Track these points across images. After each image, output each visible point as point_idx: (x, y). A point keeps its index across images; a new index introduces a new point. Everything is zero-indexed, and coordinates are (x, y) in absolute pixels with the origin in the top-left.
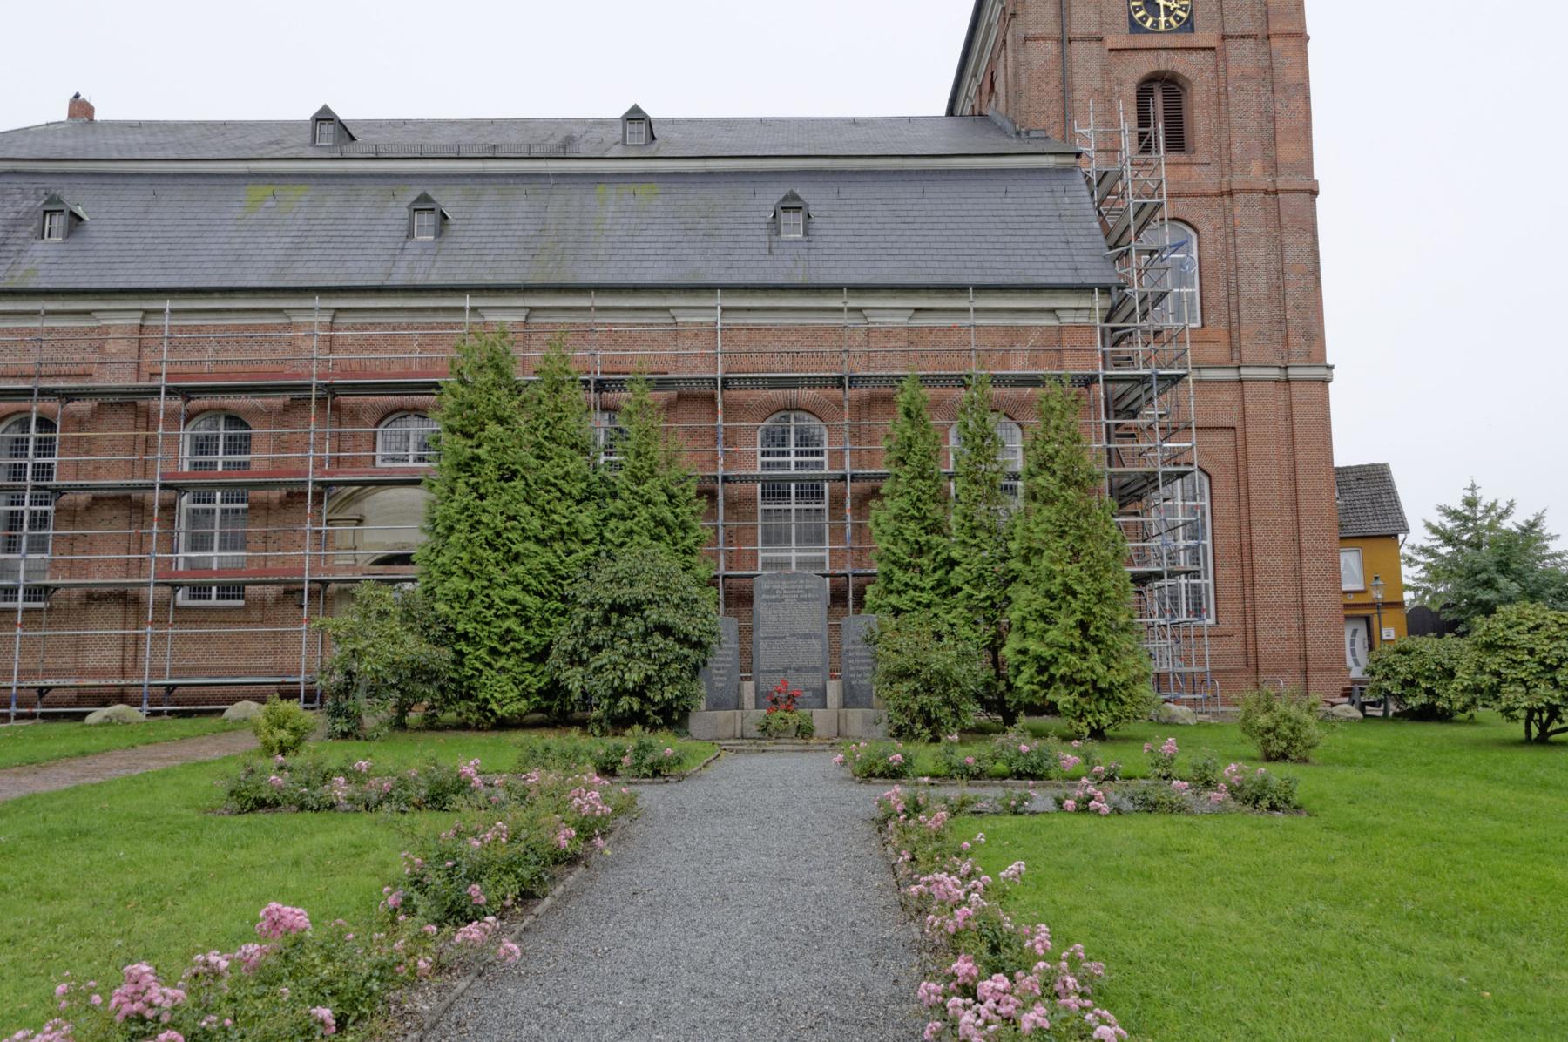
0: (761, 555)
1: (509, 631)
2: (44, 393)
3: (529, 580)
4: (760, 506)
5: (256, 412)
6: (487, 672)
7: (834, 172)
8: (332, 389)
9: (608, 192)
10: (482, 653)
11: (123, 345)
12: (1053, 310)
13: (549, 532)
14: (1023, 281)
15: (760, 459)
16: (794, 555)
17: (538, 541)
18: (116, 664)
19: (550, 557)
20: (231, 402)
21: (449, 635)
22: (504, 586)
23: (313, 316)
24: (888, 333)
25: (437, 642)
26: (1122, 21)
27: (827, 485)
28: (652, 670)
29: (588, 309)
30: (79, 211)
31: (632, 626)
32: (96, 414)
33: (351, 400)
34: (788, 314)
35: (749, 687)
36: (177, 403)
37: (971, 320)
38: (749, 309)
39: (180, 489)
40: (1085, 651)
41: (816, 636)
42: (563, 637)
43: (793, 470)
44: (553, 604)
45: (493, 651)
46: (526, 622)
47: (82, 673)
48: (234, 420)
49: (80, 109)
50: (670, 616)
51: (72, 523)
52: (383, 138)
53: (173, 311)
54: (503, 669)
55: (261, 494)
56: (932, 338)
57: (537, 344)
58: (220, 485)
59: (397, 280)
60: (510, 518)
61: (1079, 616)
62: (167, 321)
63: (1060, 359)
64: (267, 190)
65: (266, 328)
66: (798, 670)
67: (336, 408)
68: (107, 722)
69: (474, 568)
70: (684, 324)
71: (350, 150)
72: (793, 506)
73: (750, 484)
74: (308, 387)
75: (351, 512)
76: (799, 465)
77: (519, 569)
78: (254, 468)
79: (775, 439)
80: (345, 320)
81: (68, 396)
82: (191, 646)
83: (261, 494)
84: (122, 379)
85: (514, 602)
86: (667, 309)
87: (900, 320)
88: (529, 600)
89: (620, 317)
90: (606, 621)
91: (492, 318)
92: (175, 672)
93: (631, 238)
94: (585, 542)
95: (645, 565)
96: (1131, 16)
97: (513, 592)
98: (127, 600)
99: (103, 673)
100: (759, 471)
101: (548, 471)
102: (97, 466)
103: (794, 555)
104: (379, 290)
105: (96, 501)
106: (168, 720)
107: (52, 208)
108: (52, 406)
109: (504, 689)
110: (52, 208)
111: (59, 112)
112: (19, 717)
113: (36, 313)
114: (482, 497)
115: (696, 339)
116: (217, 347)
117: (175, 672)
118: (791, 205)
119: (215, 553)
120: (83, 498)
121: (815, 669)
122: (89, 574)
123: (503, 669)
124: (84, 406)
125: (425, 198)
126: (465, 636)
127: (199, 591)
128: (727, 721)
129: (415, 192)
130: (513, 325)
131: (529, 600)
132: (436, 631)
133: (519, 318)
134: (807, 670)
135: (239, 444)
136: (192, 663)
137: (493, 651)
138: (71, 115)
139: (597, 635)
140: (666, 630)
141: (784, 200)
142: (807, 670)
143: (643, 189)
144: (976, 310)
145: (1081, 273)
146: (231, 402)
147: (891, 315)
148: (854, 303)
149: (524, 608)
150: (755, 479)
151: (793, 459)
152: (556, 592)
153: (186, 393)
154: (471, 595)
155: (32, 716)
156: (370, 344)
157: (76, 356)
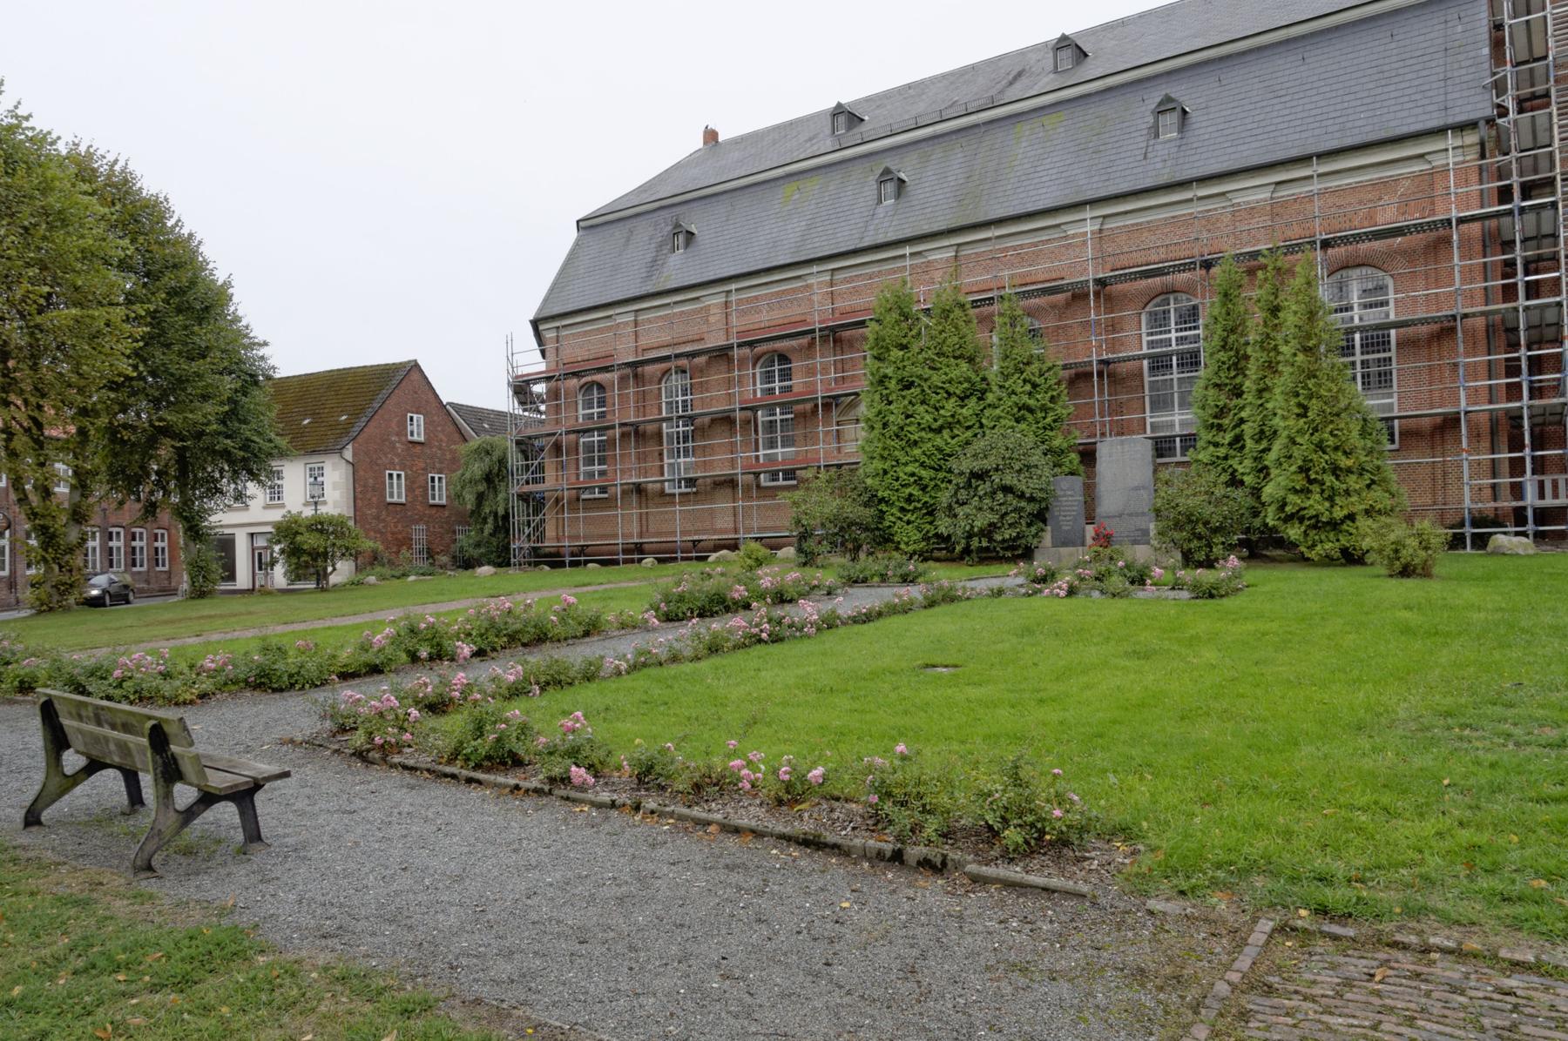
0: (1149, 421)
1: (911, 495)
2: (677, 356)
3: (923, 458)
4: (1147, 379)
5: (794, 349)
6: (899, 523)
7: (1221, 59)
8: (833, 329)
9: (1024, 128)
10: (894, 510)
11: (717, 317)
12: (1421, 156)
13: (940, 422)
14: (1383, 135)
15: (1145, 339)
16: (1177, 418)
17: (931, 430)
18: (731, 525)
19: (939, 441)
20: (778, 345)
21: (873, 500)
22: (906, 464)
23: (817, 278)
24: (1252, 210)
25: (866, 505)
27: (1393, 332)
28: (994, 518)
29: (1191, 200)
30: (693, 229)
31: (984, 488)
32: (708, 363)
33: (848, 333)
34: (1158, 213)
35: (1090, 530)
36: (746, 351)
37: (1316, 186)
38: (1126, 213)
39: (754, 409)
40: (1309, 491)
41: (1144, 488)
42: (944, 497)
43: (1174, 347)
44: (941, 475)
45: (902, 509)
46: (924, 489)
47: (715, 532)
48: (783, 358)
49: (711, 136)
50: (1009, 479)
51: (703, 437)
52: (646, 197)
53: (912, 254)
54: (908, 523)
55: (800, 407)
56: (1297, 206)
57: (930, 279)
58: (779, 404)
59: (866, 243)
60: (908, 417)
61: (1300, 463)
62: (908, 262)
63: (1433, 203)
64: (794, 186)
65: (794, 290)
66: (1130, 515)
67: (1109, 298)
68: (718, 561)
69: (886, 453)
70: (1074, 236)
71: (863, 128)
72: (1175, 376)
73: (1137, 363)
74: (813, 331)
75: (852, 415)
76: (1180, 340)
77: (917, 452)
78: (795, 390)
79: (1159, 321)
80: (839, 276)
81: (692, 355)
82: (770, 513)
83: (800, 407)
84: (715, 340)
85: (913, 475)
86: (1058, 226)
87: (1264, 195)
88: (924, 473)
89: (1022, 238)
90: (969, 485)
91: (1239, 199)
92: (585, 538)
93: (1036, 170)
94: (968, 428)
95: (1004, 440)
97: (909, 469)
98: (731, 483)
99: (725, 531)
100: (1145, 351)
101: (937, 379)
102: (712, 398)
103: (1177, 418)
104: (1304, 160)
105: (713, 421)
106: (694, 562)
107: (677, 229)
108: (684, 362)
109: (908, 535)
110: (677, 229)
111: (698, 143)
112: (683, 559)
113: (989, 239)
114: (890, 403)
115: (1078, 251)
116: (766, 311)
117: (760, 529)
118: (1167, 106)
119: (779, 450)
120: (707, 419)
121: (1143, 514)
122: (714, 469)
123: (908, 523)
124: (702, 360)
125: (887, 171)
126: (882, 500)
127: (774, 476)
128: (1071, 555)
129: (1154, 97)
130: (947, 260)
131: (924, 473)
132: (865, 497)
133: (721, 299)
134: (1137, 515)
135: (786, 375)
136: (771, 524)
137: (902, 509)
138: (705, 143)
139: (963, 495)
140: (1007, 489)
141: (1160, 104)
142: (1137, 515)
143: (1049, 120)
144: (1319, 175)
145: (1450, 112)
146: (598, 377)
147: (1254, 192)
148: (1323, 169)
149: (921, 479)
150: (1144, 357)
151: (1173, 335)
152: (940, 463)
153: (751, 344)
154: (885, 472)
155: (690, 559)
156: (856, 291)
157: (793, 312)
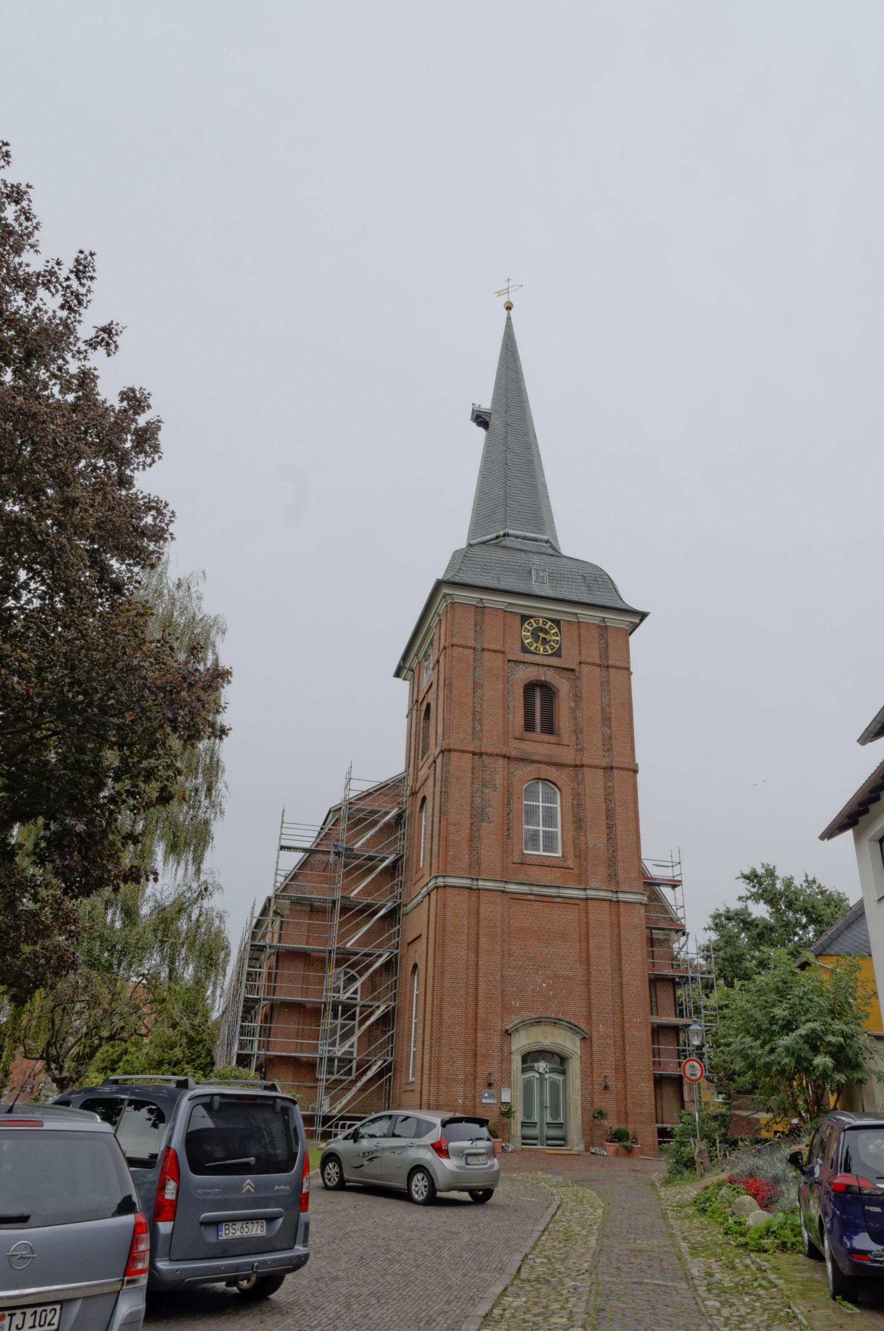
26: (518, 647)
96: (523, 642)
